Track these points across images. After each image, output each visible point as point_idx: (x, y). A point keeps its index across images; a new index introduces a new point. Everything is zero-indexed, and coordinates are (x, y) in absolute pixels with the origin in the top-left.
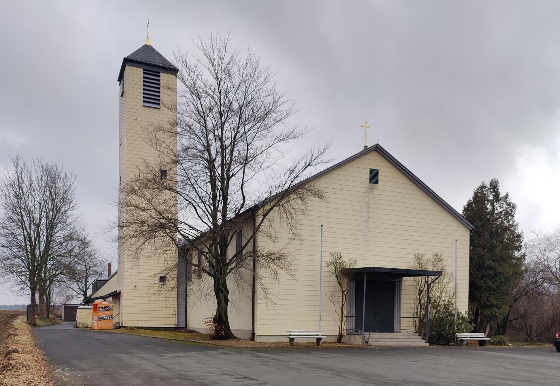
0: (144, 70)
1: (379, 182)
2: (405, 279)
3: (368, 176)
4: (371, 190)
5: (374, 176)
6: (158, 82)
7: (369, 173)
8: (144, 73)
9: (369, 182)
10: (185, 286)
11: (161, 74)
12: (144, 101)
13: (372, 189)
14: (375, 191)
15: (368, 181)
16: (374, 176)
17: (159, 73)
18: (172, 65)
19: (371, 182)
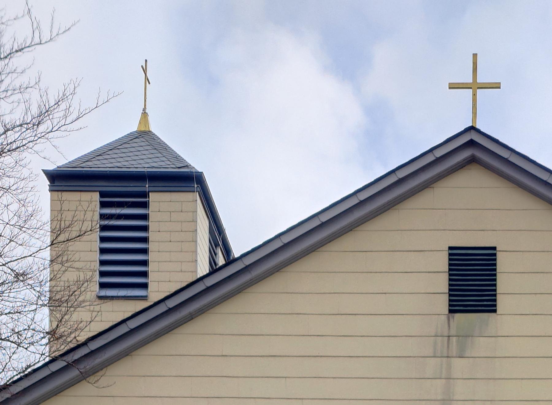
0: (102, 195)
1: (502, 302)
2: (224, 262)
3: (442, 283)
4: (456, 347)
5: (472, 281)
6: (106, 222)
7: (445, 267)
8: (103, 205)
9: (445, 308)
10: (190, 270)
11: (153, 197)
12: (103, 286)
13: (465, 336)
14: (481, 346)
15: (442, 303)
16: (472, 281)
17: (145, 195)
18: (187, 166)
19: (457, 305)
